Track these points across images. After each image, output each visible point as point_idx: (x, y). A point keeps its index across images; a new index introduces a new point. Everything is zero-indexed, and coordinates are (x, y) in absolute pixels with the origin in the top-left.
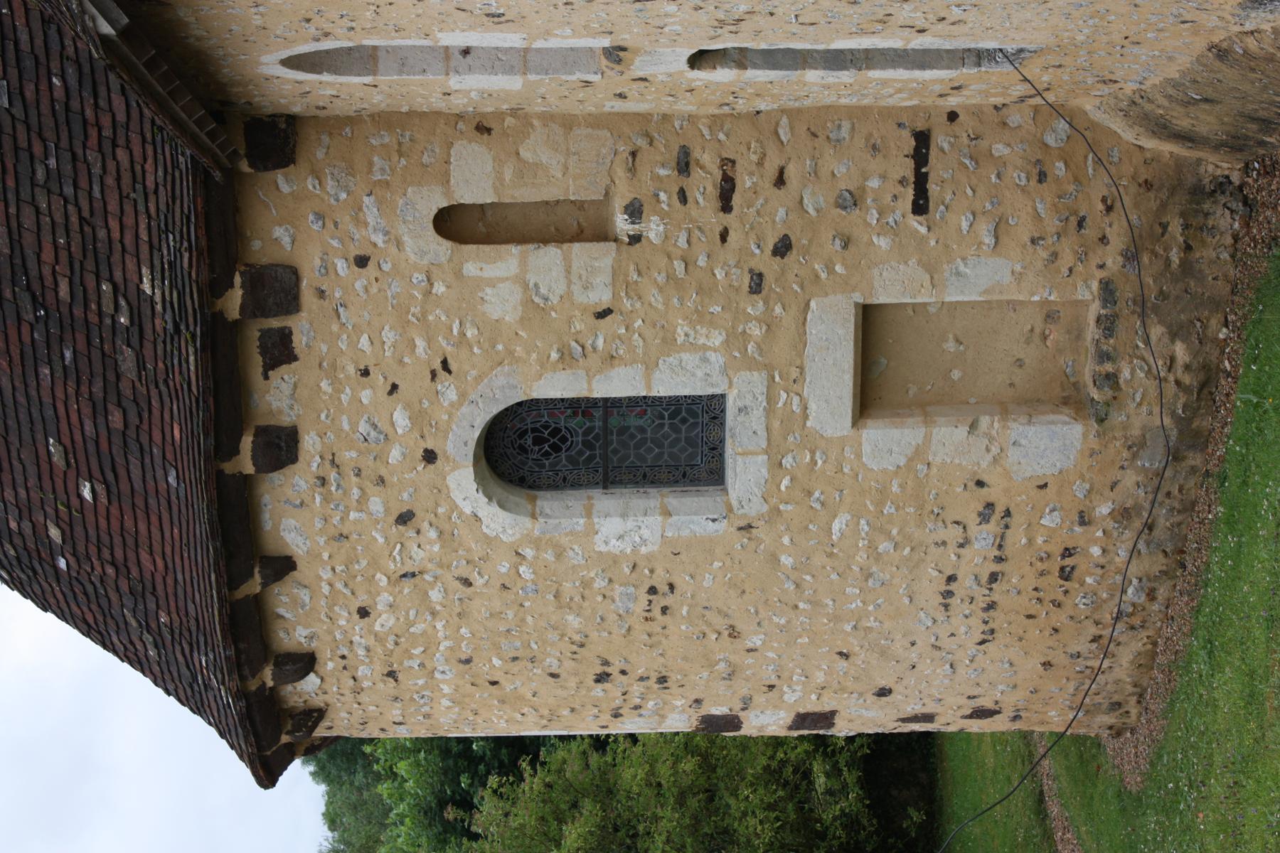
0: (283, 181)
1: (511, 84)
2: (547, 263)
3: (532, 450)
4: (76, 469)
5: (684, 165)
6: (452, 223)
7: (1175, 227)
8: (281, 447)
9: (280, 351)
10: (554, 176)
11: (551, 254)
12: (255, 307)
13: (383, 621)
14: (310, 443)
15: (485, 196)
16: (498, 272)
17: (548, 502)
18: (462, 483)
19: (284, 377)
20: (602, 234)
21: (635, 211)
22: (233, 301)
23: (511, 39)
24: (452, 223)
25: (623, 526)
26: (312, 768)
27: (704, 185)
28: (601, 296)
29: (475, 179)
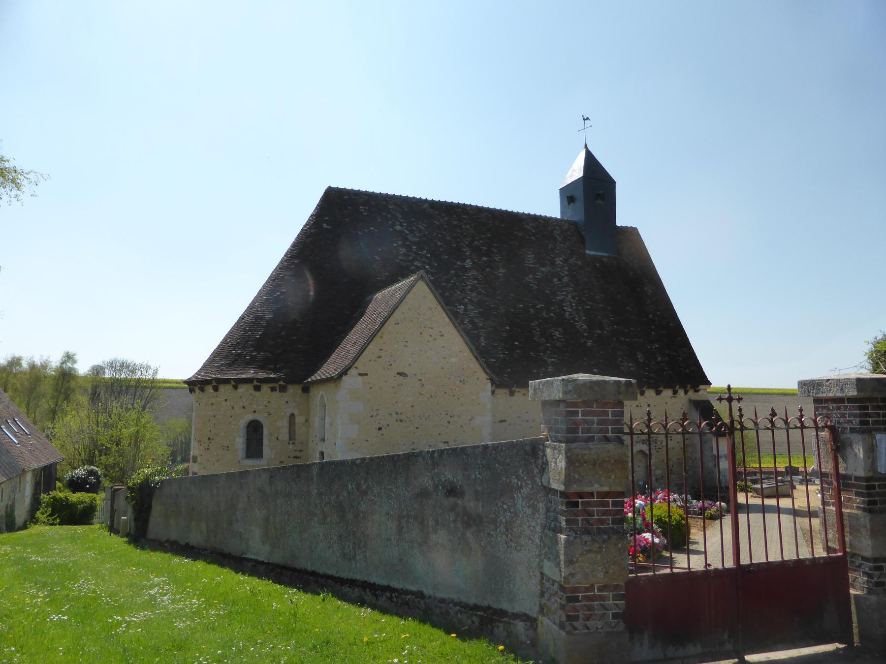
0: (300, 391)
1: (316, 425)
2: (285, 430)
3: (254, 430)
4: (252, 357)
5: (300, 451)
6: (292, 416)
7: (505, 619)
8: (257, 388)
9: (273, 389)
10: (300, 431)
11: (287, 431)
12: (280, 386)
13: (224, 403)
14: (258, 393)
15: (297, 421)
16: (284, 424)
17: (245, 430)
18: (250, 417)
19: (269, 390)
20: (290, 439)
21: (293, 444)
22: (282, 383)
23: (327, 425)
24: (292, 416)
25: (240, 442)
26: (25, 365)
27: (297, 454)
28: (280, 438)
29: (299, 420)
